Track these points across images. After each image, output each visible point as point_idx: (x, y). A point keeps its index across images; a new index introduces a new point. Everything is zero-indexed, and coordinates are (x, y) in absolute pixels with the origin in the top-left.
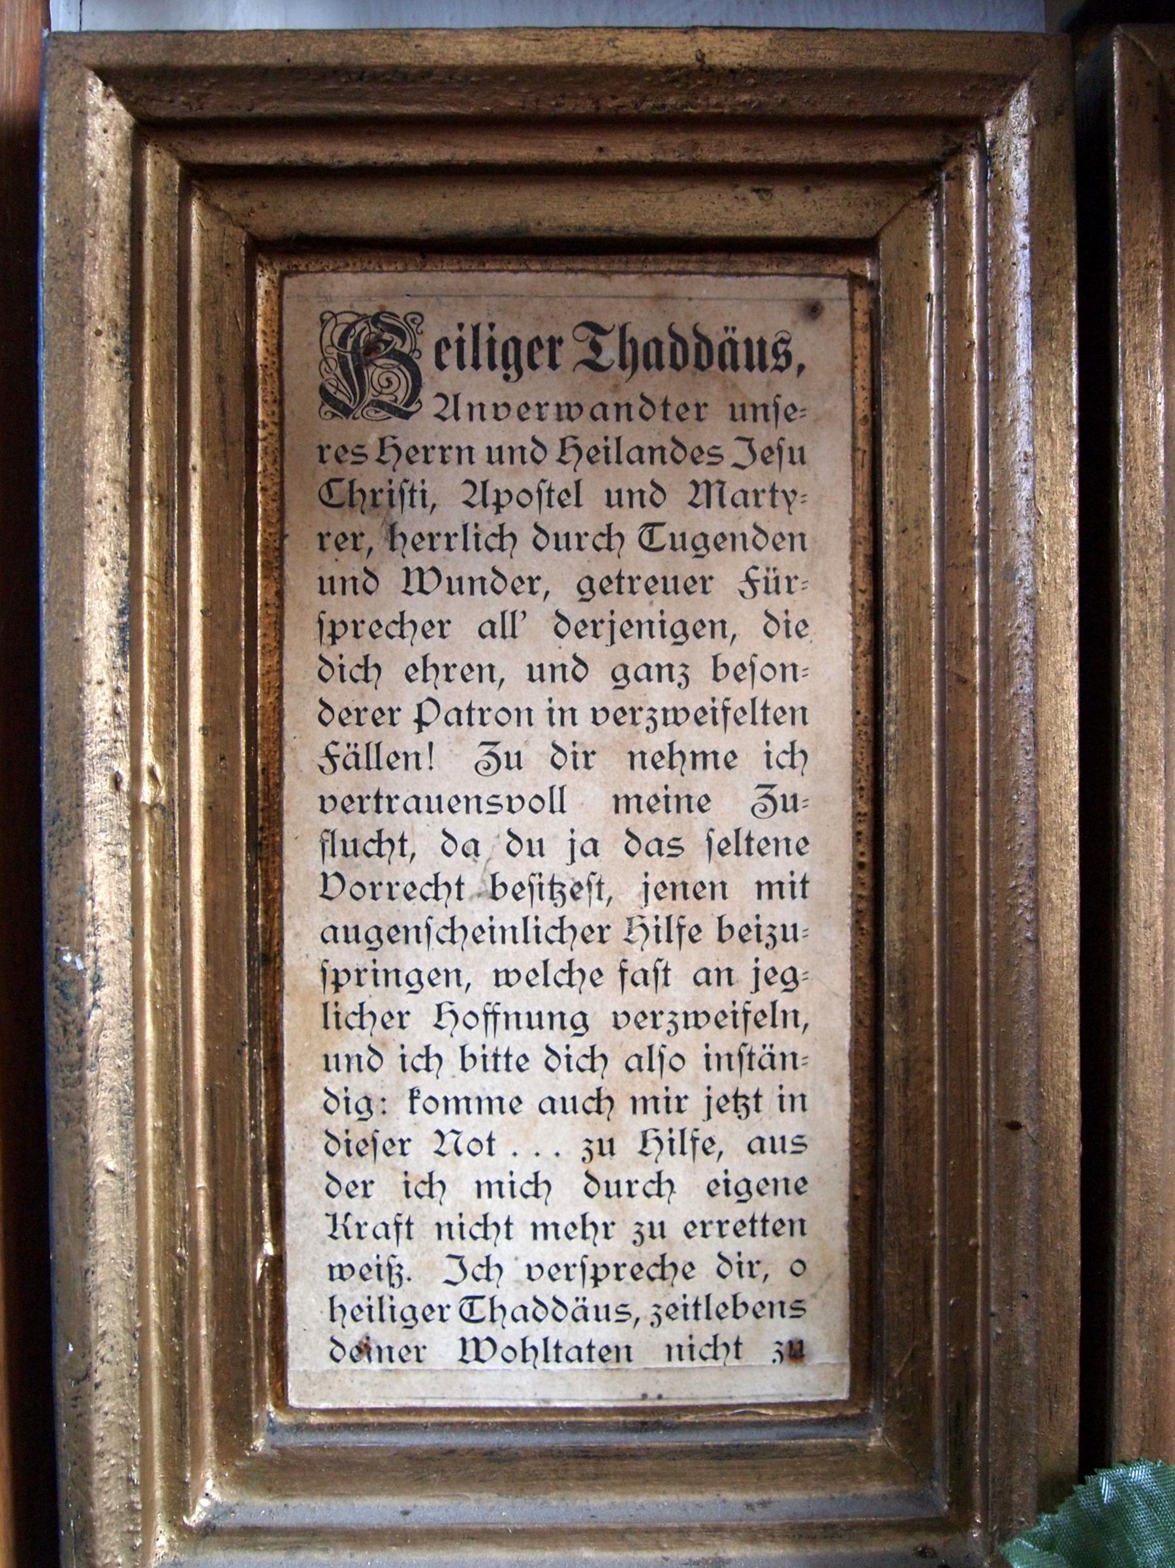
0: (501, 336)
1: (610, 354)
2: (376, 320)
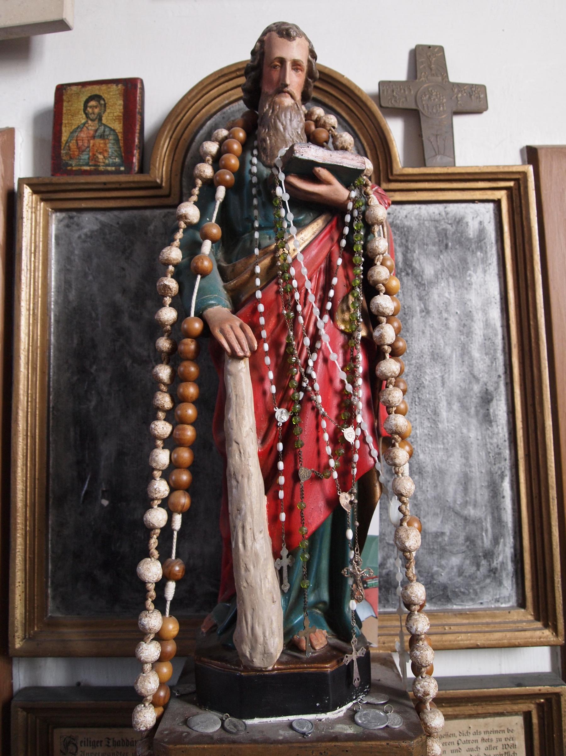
0: (92, 740)
1: (111, 744)
2: (70, 737)
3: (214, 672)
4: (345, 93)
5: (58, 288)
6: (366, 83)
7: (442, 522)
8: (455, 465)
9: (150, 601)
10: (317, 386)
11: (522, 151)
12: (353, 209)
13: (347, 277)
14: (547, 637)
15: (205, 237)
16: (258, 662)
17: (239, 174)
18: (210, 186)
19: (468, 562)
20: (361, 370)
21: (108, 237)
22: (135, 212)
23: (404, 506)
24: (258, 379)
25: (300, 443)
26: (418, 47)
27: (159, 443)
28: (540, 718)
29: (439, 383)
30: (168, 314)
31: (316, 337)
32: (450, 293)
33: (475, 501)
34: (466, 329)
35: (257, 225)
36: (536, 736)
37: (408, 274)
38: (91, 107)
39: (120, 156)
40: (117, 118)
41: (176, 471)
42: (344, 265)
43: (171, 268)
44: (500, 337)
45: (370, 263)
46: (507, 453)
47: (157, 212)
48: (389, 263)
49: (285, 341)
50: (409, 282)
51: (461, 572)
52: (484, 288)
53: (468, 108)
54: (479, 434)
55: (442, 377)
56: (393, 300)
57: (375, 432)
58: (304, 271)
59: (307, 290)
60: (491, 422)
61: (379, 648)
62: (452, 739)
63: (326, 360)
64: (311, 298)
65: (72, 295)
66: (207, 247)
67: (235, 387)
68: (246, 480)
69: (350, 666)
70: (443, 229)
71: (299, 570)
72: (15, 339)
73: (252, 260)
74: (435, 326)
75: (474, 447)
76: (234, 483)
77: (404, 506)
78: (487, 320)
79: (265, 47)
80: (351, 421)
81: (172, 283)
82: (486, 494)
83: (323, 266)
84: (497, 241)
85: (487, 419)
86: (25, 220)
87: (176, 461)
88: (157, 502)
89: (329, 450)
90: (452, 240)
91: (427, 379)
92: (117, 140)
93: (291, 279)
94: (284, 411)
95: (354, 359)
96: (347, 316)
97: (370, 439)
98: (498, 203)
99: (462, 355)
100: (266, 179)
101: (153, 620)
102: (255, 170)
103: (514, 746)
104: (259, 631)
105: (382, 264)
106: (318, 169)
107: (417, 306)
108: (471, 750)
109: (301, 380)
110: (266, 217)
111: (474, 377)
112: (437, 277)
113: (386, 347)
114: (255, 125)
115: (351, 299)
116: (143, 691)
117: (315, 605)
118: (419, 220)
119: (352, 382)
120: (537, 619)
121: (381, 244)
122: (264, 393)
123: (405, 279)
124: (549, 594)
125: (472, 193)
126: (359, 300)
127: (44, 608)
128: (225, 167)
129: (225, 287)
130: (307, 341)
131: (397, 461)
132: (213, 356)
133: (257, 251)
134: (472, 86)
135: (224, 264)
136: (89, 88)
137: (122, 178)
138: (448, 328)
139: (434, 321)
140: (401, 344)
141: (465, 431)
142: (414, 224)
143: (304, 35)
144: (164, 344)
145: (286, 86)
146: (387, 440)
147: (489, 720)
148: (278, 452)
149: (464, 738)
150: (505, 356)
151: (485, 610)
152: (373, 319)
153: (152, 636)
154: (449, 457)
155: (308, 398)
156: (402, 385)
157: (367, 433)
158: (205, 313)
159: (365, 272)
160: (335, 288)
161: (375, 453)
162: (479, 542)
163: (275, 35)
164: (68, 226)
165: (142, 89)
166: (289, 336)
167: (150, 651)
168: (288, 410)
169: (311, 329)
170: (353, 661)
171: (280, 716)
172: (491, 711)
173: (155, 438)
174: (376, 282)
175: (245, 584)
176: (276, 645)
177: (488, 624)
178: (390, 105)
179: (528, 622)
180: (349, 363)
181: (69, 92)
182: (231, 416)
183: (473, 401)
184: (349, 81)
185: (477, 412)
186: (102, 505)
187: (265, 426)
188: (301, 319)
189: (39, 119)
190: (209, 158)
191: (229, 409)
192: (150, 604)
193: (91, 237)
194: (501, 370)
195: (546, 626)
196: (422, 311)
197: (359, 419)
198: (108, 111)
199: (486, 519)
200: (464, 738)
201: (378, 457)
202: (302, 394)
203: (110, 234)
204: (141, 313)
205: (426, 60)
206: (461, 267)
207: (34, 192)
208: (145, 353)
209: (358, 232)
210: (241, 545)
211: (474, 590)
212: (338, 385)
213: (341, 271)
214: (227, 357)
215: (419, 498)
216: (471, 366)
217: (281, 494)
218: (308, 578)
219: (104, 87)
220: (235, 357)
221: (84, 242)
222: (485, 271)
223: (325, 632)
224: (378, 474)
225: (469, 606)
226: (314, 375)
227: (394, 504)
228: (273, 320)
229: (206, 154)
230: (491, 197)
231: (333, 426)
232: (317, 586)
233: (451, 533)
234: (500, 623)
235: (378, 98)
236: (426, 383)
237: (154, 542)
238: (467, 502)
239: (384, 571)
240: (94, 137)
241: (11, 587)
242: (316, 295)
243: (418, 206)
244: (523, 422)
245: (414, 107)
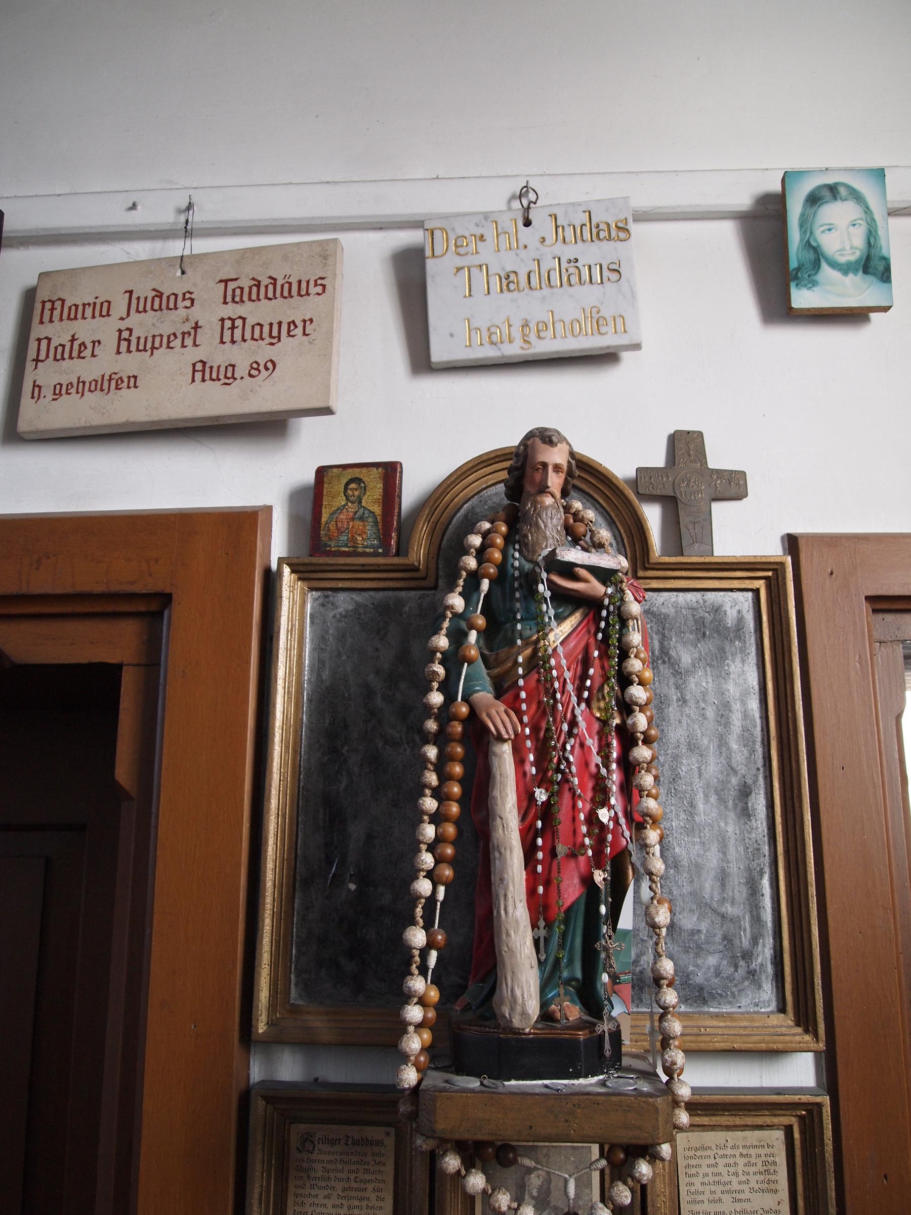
1: (350, 1142)
3: (474, 1036)
4: (602, 481)
5: (311, 666)
6: (621, 466)
7: (698, 919)
8: (713, 859)
9: (414, 965)
10: (574, 769)
11: (782, 538)
12: (609, 604)
13: (603, 667)
14: (807, 1042)
15: (471, 627)
16: (517, 1023)
17: (502, 567)
18: (474, 578)
19: (725, 962)
20: (615, 755)
21: (363, 616)
22: (390, 593)
23: (654, 885)
24: (520, 762)
25: (557, 821)
26: (676, 432)
27: (426, 818)
28: (802, 1132)
29: (696, 774)
30: (436, 698)
31: (573, 723)
32: (707, 682)
33: (734, 898)
34: (723, 719)
35: (519, 617)
36: (798, 1153)
37: (664, 662)
38: (351, 489)
39: (378, 538)
40: (376, 501)
41: (441, 845)
42: (600, 656)
43: (439, 655)
44: (759, 729)
45: (624, 655)
46: (766, 849)
47: (413, 593)
48: (642, 656)
49: (544, 725)
50: (665, 670)
51: (718, 974)
52: (744, 676)
53: (727, 495)
54: (737, 828)
55: (699, 768)
56: (646, 690)
57: (628, 815)
58: (564, 662)
59: (565, 680)
60: (749, 816)
61: (631, 1047)
62: (708, 1153)
63: (582, 745)
64: (570, 687)
65: (326, 674)
66: (473, 636)
67: (500, 767)
68: (509, 852)
69: (601, 1037)
70: (701, 617)
71: (556, 939)
72: (271, 717)
73: (515, 650)
74: (692, 715)
75: (732, 841)
76: (497, 854)
77: (654, 885)
78: (745, 711)
79: (529, 451)
80: (605, 803)
81: (440, 670)
82: (745, 891)
83: (580, 657)
84: (755, 631)
85: (746, 813)
86: (284, 599)
87: (442, 835)
88: (423, 874)
89: (584, 829)
90: (710, 629)
91: (683, 770)
92: (376, 523)
93: (551, 669)
94: (543, 791)
95: (609, 745)
96: (602, 704)
97: (622, 821)
98: (756, 592)
99: (720, 746)
100: (527, 574)
101: (418, 984)
102: (517, 564)
103: (775, 1163)
104: (518, 993)
105: (636, 657)
106: (577, 569)
107: (674, 695)
108: (729, 1165)
109: (559, 762)
110: (527, 610)
111: (732, 768)
112: (694, 665)
113: (639, 734)
114: (517, 518)
115: (606, 689)
116: (408, 1050)
117: (568, 982)
118: (676, 607)
119: (607, 766)
120: (798, 1024)
121: (635, 638)
122: (525, 774)
123: (661, 667)
124: (809, 997)
125: (730, 581)
126: (613, 689)
127: (287, 993)
128: (489, 561)
129: (488, 674)
130: (565, 727)
131: (648, 842)
132: (479, 738)
133: (519, 642)
134: (731, 472)
135: (486, 652)
136: (350, 470)
137: (381, 560)
138: (705, 718)
139: (691, 710)
140: (653, 732)
141: (722, 825)
142: (671, 611)
143: (565, 439)
144: (432, 725)
145: (548, 487)
146: (638, 823)
147: (748, 1133)
148: (537, 829)
149: (721, 1152)
150: (764, 748)
151: (743, 1013)
152: (627, 707)
153: (416, 1000)
154: (706, 851)
155: (566, 780)
156: (654, 771)
157: (620, 815)
158: (471, 698)
159: (620, 664)
160: (591, 678)
161: (627, 834)
162: (737, 942)
163: (538, 441)
164: (323, 605)
165: (401, 472)
166: (548, 721)
167: (414, 1013)
168: (547, 790)
169: (569, 715)
170: (604, 1031)
171: (535, 1080)
172: (749, 1123)
173: (423, 812)
174: (630, 674)
175: (506, 949)
176: (533, 1008)
177: (745, 1027)
178: (648, 492)
179: (789, 1027)
180: (604, 748)
181: (330, 474)
182: (496, 793)
183: (731, 794)
184: (606, 469)
185: (735, 805)
186: (349, 889)
187: (525, 804)
188: (560, 706)
189: (296, 496)
190: (472, 550)
191: (493, 787)
192: (414, 969)
193: (346, 617)
194: (760, 763)
195: (806, 1031)
196: (678, 700)
197: (613, 801)
198: (368, 494)
199: (744, 918)
200: (721, 1152)
201: (631, 838)
202: (560, 776)
203: (365, 614)
204: (394, 695)
205: (685, 446)
206: (719, 656)
207: (293, 572)
208: (398, 735)
209: (614, 626)
210: (502, 912)
211: (732, 992)
212: (593, 769)
213: (597, 662)
214: (492, 739)
215: (675, 893)
216: (729, 758)
217: (539, 868)
218: (563, 948)
219: (364, 470)
220: (500, 739)
221: (339, 621)
222: (743, 661)
223: (577, 1007)
224: (631, 855)
225: (726, 1009)
226: (571, 759)
227: (645, 884)
228: (534, 706)
229: (470, 547)
230: (750, 587)
231: (588, 806)
232: (571, 962)
233: (707, 931)
234: (758, 1027)
235: (634, 483)
236: (683, 774)
237: (419, 911)
238: (724, 898)
239: (638, 969)
240: (353, 519)
241: (257, 969)
242: (573, 684)
243: (675, 593)
244: (782, 816)
245: (672, 494)
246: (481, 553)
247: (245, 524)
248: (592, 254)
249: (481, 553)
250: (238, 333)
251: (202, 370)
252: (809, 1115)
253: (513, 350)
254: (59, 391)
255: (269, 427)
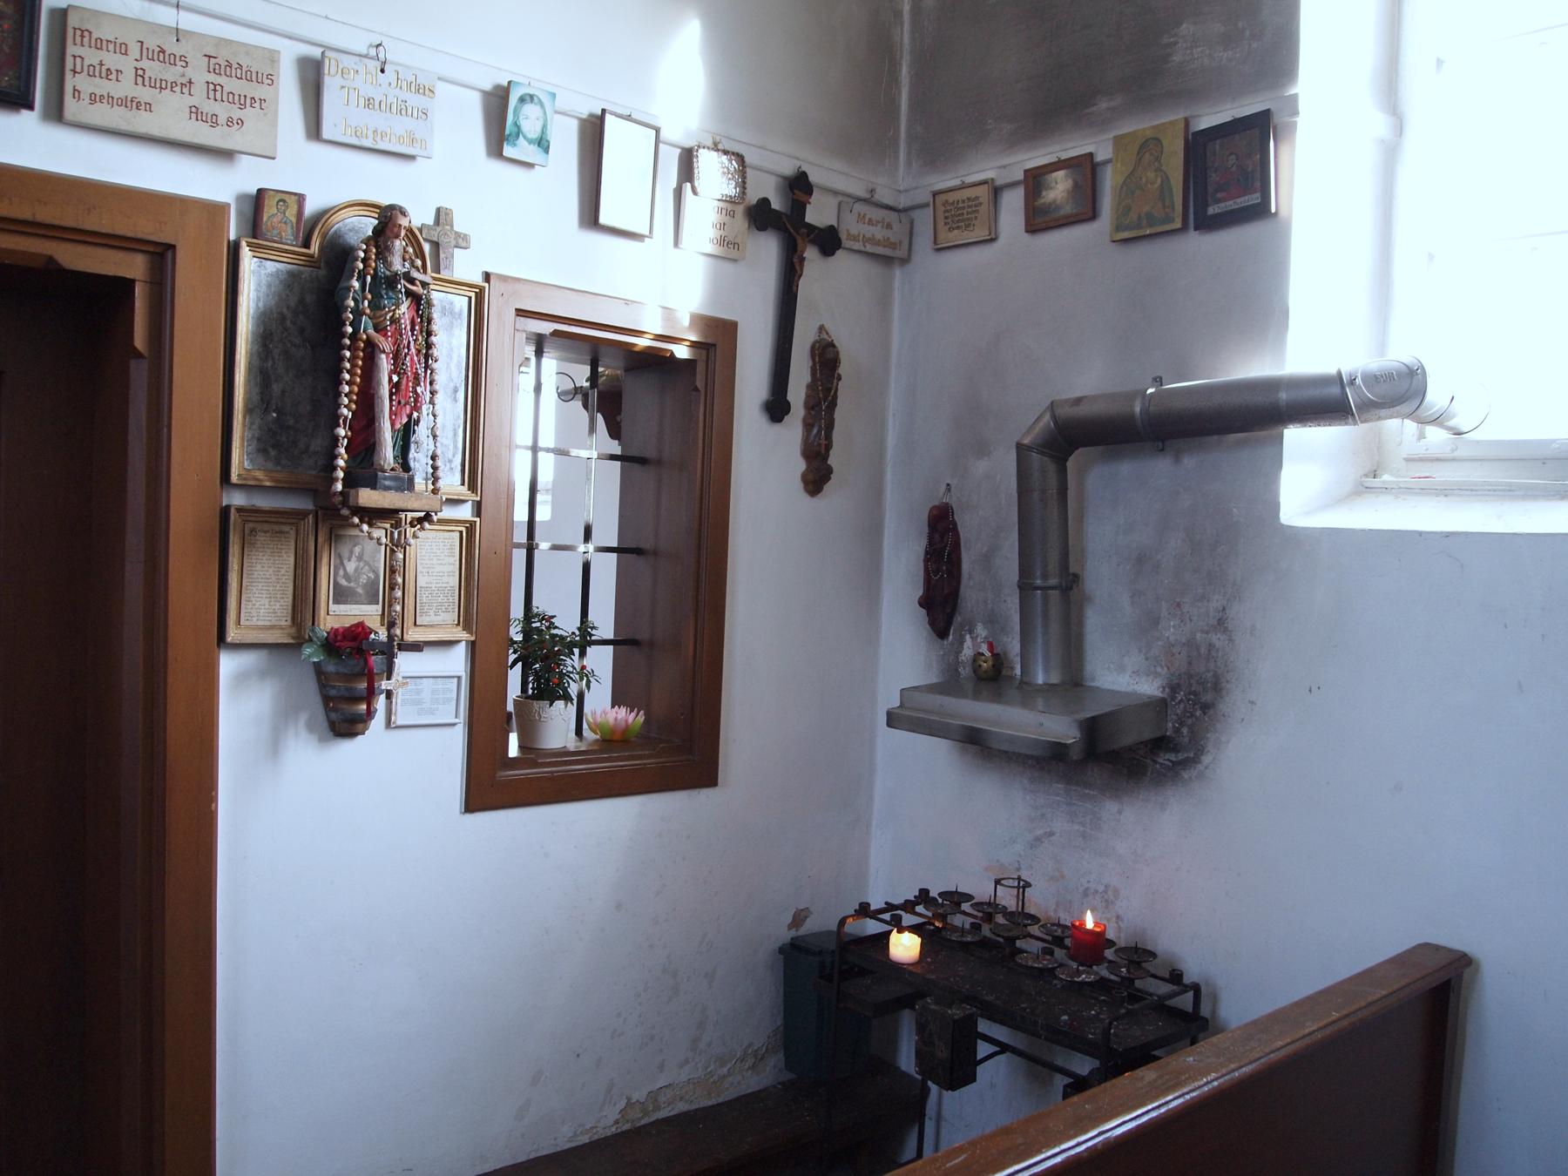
85: (455, 400)
246: (364, 261)
247: (215, 211)
248: (415, 101)
249: (364, 261)
250: (218, 95)
251: (195, 112)
252: (471, 528)
253: (368, 143)
254: (94, 99)
255: (226, 155)
